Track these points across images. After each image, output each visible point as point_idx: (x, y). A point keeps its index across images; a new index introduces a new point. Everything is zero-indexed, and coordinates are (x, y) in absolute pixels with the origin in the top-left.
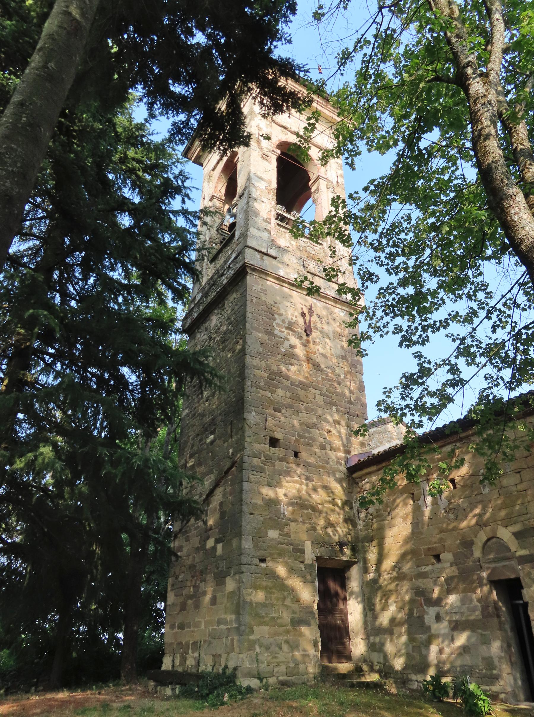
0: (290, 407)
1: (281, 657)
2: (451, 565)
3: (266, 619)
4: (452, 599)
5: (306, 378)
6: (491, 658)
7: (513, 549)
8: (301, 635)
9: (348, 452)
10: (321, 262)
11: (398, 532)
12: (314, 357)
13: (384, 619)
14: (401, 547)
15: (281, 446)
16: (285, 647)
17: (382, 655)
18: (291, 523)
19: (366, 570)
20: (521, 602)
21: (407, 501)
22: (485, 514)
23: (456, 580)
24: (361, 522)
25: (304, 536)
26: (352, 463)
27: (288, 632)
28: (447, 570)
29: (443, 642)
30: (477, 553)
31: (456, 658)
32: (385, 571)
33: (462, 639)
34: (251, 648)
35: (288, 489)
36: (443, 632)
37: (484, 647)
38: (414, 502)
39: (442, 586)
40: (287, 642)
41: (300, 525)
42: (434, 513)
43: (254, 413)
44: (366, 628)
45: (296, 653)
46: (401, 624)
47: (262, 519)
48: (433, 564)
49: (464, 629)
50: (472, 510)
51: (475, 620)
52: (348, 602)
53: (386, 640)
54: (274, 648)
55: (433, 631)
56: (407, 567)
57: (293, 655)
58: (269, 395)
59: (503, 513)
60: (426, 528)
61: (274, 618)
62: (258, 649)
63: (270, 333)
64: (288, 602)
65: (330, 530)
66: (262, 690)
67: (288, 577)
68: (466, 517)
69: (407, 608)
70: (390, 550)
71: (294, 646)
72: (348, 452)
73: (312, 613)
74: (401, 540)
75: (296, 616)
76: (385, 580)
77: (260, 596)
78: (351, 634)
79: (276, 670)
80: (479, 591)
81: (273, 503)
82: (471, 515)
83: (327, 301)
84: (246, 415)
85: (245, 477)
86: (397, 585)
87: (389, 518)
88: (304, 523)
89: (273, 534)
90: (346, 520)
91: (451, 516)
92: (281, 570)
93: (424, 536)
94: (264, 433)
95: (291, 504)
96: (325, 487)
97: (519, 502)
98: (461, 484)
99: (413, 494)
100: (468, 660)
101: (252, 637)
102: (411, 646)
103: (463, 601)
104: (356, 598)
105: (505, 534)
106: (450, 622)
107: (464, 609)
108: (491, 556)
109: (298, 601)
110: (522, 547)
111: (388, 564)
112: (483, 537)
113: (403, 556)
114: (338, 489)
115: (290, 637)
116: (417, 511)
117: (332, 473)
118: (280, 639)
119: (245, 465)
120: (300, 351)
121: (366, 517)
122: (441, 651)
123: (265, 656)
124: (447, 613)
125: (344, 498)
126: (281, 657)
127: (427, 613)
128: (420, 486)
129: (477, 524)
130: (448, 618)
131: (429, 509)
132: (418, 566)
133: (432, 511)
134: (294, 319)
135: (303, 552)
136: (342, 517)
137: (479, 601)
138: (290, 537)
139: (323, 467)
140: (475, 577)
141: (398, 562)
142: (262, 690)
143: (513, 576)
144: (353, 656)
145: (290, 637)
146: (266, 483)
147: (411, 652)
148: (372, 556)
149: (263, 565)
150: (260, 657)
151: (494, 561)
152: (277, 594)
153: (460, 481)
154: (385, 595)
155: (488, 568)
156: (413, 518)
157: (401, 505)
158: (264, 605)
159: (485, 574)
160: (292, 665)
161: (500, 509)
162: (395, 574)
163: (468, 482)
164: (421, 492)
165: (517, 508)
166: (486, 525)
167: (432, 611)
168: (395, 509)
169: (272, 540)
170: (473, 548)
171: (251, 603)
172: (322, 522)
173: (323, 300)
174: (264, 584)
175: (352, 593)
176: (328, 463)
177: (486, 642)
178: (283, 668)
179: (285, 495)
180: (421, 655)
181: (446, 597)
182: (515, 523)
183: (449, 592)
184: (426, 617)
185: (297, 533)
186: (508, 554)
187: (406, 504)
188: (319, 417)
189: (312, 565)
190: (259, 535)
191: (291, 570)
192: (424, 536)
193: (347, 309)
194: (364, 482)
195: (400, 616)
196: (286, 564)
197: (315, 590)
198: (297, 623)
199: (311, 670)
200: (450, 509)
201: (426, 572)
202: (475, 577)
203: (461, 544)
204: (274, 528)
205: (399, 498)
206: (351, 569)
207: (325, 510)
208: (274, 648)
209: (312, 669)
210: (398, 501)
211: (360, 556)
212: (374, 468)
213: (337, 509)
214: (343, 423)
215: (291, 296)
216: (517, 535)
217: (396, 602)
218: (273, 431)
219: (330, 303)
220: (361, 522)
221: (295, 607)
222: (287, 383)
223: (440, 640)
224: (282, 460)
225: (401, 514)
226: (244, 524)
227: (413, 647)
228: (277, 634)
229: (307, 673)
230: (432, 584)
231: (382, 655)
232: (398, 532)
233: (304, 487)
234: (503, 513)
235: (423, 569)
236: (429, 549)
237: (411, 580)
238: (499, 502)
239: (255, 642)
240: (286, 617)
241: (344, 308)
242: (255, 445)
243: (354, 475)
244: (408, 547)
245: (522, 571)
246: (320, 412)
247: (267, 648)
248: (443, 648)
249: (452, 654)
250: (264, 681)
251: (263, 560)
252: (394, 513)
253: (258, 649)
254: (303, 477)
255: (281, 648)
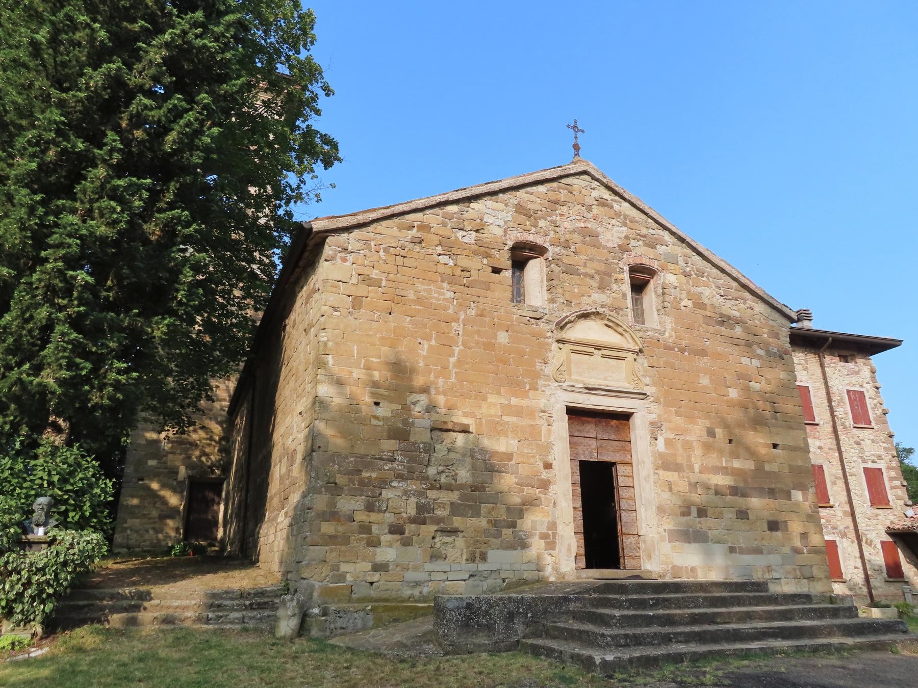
1: (147, 537)
8: (166, 524)
10: (891, 436)
16: (151, 532)
20: (321, 426)
40: (154, 529)
41: (177, 456)
64: (158, 505)
65: (204, 459)
66: (23, 210)
67: (160, 490)
88: (181, 454)
89: (152, 463)
90: (220, 451)
92: (155, 486)
101: (125, 525)
115: (157, 526)
117: (214, 418)
118: (147, 526)
126: (147, 537)
142: (23, 210)
172: (197, 453)
190: (140, 463)
196: (159, 481)
198: (163, 517)
204: (153, 458)
213: (213, 443)
221: (163, 507)
239: (127, 528)
240: (155, 514)
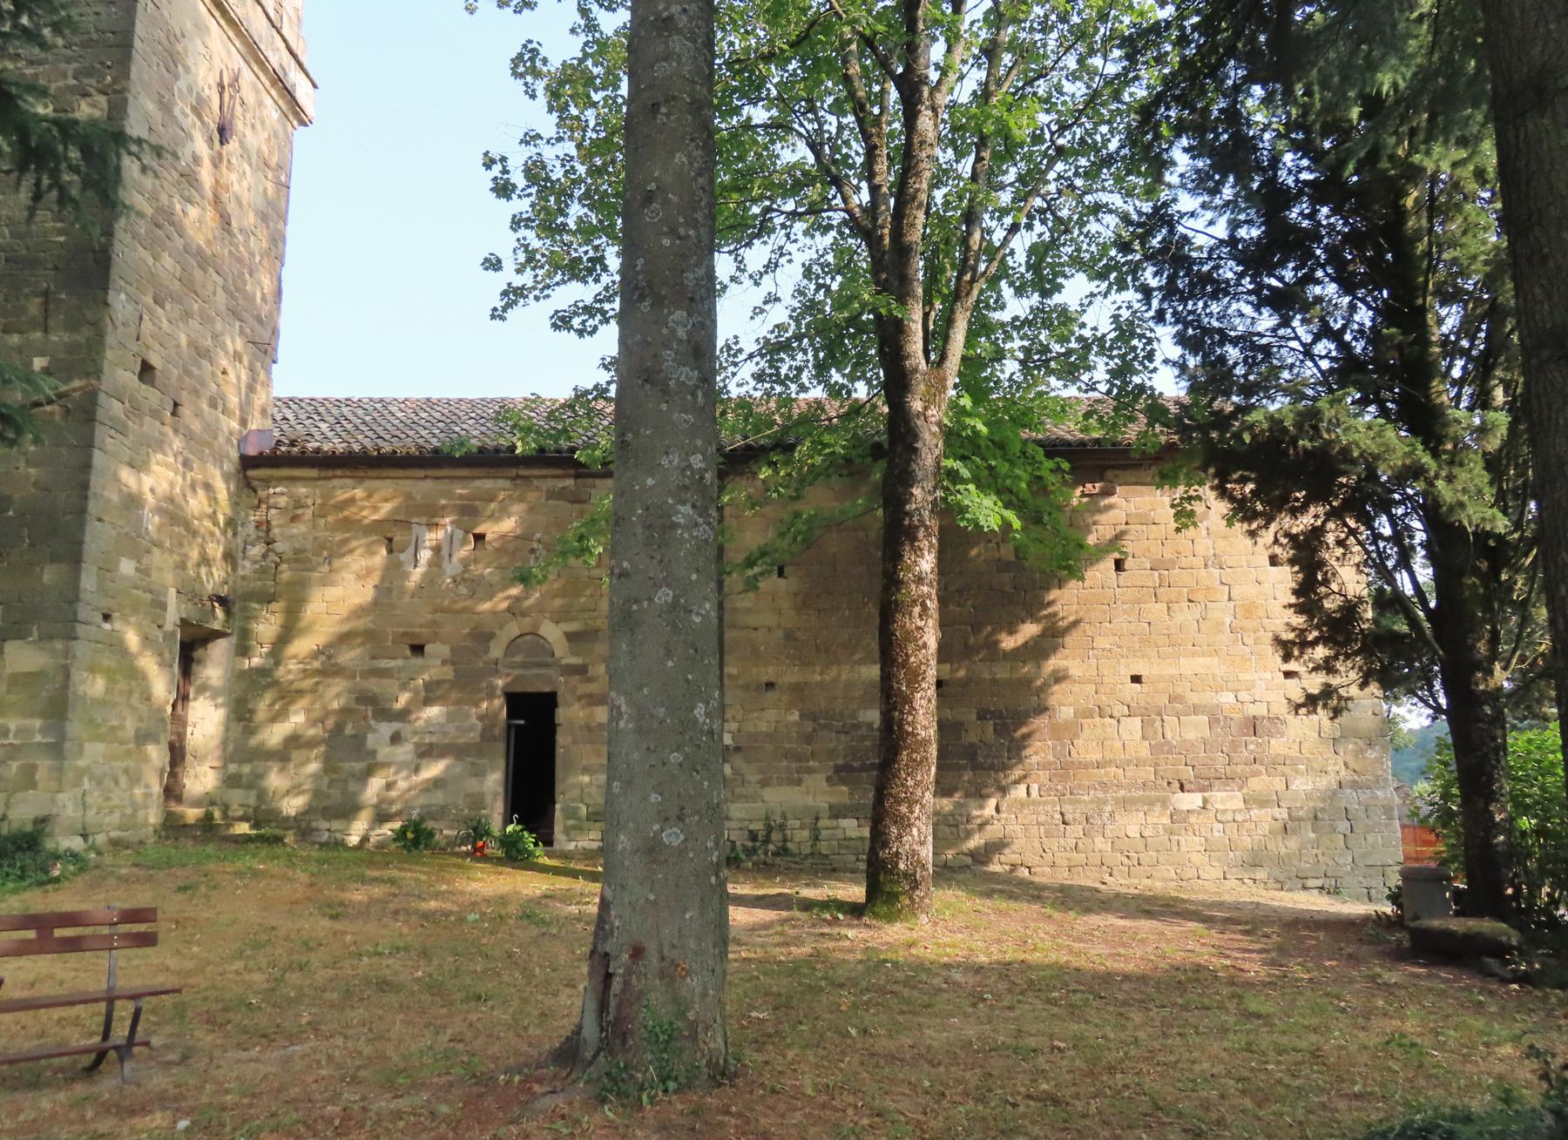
0: (180, 302)
2: (444, 663)
3: (103, 730)
4: (434, 712)
5: (209, 242)
6: (481, 795)
7: (558, 654)
9: (243, 422)
11: (342, 595)
12: (225, 197)
13: (275, 735)
14: (342, 621)
15: (157, 382)
16: (123, 780)
17: (253, 793)
18: (155, 550)
19: (243, 650)
21: (374, 548)
22: (526, 598)
23: (447, 686)
24: (247, 564)
25: (169, 578)
26: (252, 451)
27: (128, 754)
28: (433, 667)
29: (396, 773)
30: (496, 651)
31: (417, 796)
32: (294, 657)
33: (434, 769)
34: (77, 783)
35: (157, 479)
36: (401, 758)
37: (474, 781)
38: (390, 551)
39: (416, 692)
40: (126, 771)
41: (167, 556)
42: (430, 579)
43: (123, 296)
44: (224, 750)
45: (136, 791)
46: (311, 744)
47: (114, 533)
48: (406, 658)
49: (441, 756)
50: (505, 588)
51: (468, 745)
52: (192, 704)
53: (270, 768)
54: (108, 782)
55: (380, 757)
56: (349, 656)
57: (132, 795)
58: (150, 261)
59: (558, 602)
60: (407, 599)
61: (113, 728)
62: (86, 784)
63: (166, 107)
68: (491, 598)
69: (330, 723)
70: (313, 623)
71: (135, 778)
72: (243, 422)
73: (163, 720)
74: (344, 610)
75: (143, 725)
76: (289, 672)
77: (97, 686)
78: (188, 757)
79: (107, 820)
80: (485, 705)
81: (133, 502)
82: (501, 595)
83: (261, 75)
84: (111, 296)
85: (97, 440)
86: (317, 683)
87: (325, 569)
89: (127, 567)
91: (463, 590)
92: (132, 639)
93: (398, 612)
94: (134, 347)
95: (159, 510)
96: (208, 487)
97: (588, 592)
98: (496, 545)
99: (390, 540)
100: (439, 797)
102: (326, 780)
103: (450, 717)
104: (214, 697)
105: (553, 632)
106: (417, 745)
107: (451, 729)
108: (518, 659)
109: (149, 699)
110: (574, 654)
111: (302, 646)
112: (513, 629)
113: (344, 639)
114: (222, 490)
116: (394, 571)
117: (219, 459)
118: (118, 765)
119: (100, 414)
120: (206, 175)
121: (264, 556)
122: (389, 786)
123: (94, 798)
124: (415, 733)
125: (229, 512)
127: (374, 731)
128: (410, 529)
129: (509, 610)
130: (416, 739)
131: (420, 570)
132: (373, 658)
133: (425, 575)
134: (207, 91)
135: (163, 606)
136: (221, 548)
137: (481, 718)
138: (149, 575)
139: (209, 445)
140: (484, 685)
141: (330, 645)
143: (547, 689)
144: (185, 796)
145: (130, 763)
146: (127, 459)
147: (325, 788)
148: (266, 627)
149: (107, 626)
150: (88, 799)
151: (525, 665)
152: (122, 685)
153: (494, 540)
154: (283, 698)
155: (508, 675)
156: (383, 579)
157: (358, 552)
158: (102, 703)
159: (500, 683)
160: (129, 811)
161: (555, 596)
162: (316, 664)
163: (510, 547)
164: (409, 542)
165: (582, 600)
166: (523, 615)
167: (386, 729)
168: (344, 555)
169: (125, 578)
170: (491, 643)
171: (84, 698)
173: (255, 68)
174: (106, 662)
175: (202, 689)
176: (216, 438)
177: (479, 773)
178: (115, 818)
179: (152, 490)
180: (345, 793)
181: (419, 709)
182: (572, 620)
183: (427, 702)
184: (370, 736)
185: (160, 569)
186: (550, 660)
187: (371, 553)
188: (215, 337)
189: (173, 634)
191: (146, 640)
192: (398, 612)
193: (284, 107)
194: (271, 491)
195: (312, 732)
196: (139, 627)
197: (172, 680)
199: (152, 820)
200: (464, 580)
201: (388, 670)
202: (484, 685)
203: (469, 634)
205: (356, 538)
206: (210, 646)
207: (202, 530)
208: (108, 782)
209: (154, 817)
210: (354, 544)
211: (237, 623)
212: (314, 473)
214: (246, 360)
215: (207, 29)
216: (571, 637)
217: (308, 711)
218: (148, 347)
219: (263, 78)
220: (247, 564)
222: (179, 242)
223: (392, 770)
224: (155, 414)
225: (356, 567)
226: (87, 538)
227: (332, 781)
228: (114, 757)
229: (146, 824)
230: (396, 689)
231: (253, 793)
232: (342, 595)
233: (179, 479)
234: (558, 602)
235: (384, 663)
236: (405, 634)
237: (354, 677)
238: (556, 586)
239: (81, 773)
240: (131, 726)
241: (281, 102)
242: (119, 375)
243: (251, 473)
244: (360, 624)
245: (561, 684)
246: (219, 326)
247: (99, 783)
248: (395, 782)
249: (409, 789)
250: (90, 840)
251: (107, 617)
252: (337, 563)
253: (86, 784)
254: (180, 459)
255: (117, 783)
